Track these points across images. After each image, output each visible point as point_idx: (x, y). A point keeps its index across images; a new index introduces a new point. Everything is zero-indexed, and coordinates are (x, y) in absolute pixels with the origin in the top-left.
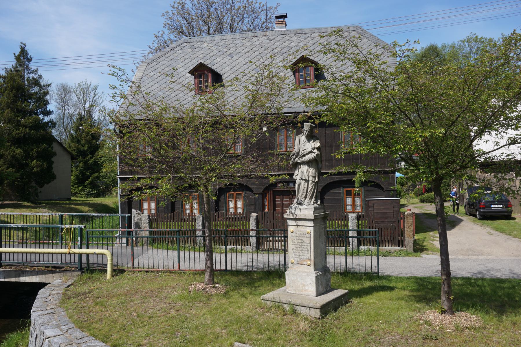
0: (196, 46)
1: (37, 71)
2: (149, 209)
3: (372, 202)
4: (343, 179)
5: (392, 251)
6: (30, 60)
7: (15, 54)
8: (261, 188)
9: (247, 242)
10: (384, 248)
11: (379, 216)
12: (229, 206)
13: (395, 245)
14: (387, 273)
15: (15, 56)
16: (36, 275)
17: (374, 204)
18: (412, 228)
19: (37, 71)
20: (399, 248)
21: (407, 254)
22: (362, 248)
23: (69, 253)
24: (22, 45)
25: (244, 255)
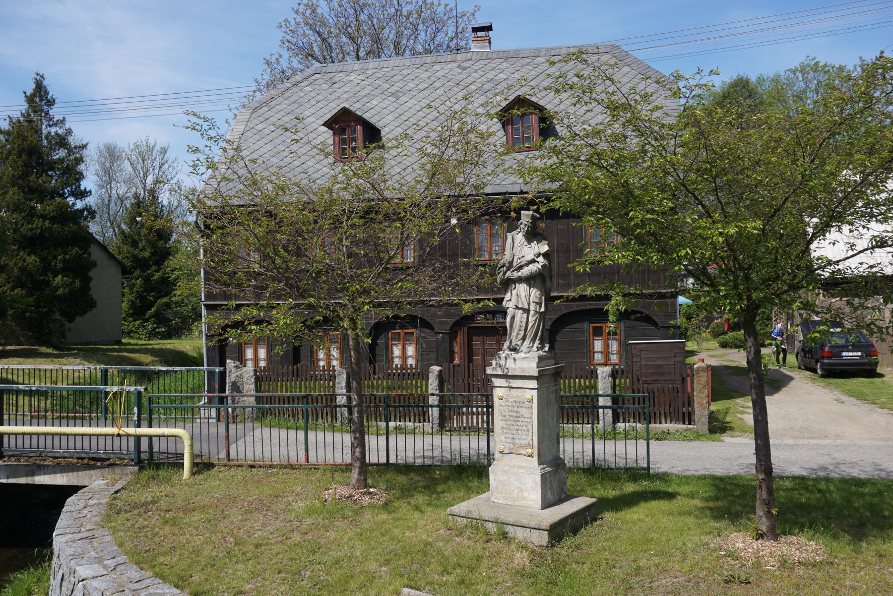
0: (336, 79)
1: (63, 121)
2: (256, 359)
3: (638, 347)
4: (588, 307)
5: (672, 431)
6: (51, 103)
7: (25, 93)
8: (447, 323)
9: (423, 416)
10: (658, 425)
11: (649, 371)
12: (392, 353)
13: (678, 421)
14: (664, 468)
15: (26, 97)
16: (62, 472)
17: (641, 350)
18: (706, 391)
19: (63, 121)
20: (684, 426)
21: (698, 437)
22: (621, 426)
23: (119, 435)
24: (38, 78)
25: (419, 439)
